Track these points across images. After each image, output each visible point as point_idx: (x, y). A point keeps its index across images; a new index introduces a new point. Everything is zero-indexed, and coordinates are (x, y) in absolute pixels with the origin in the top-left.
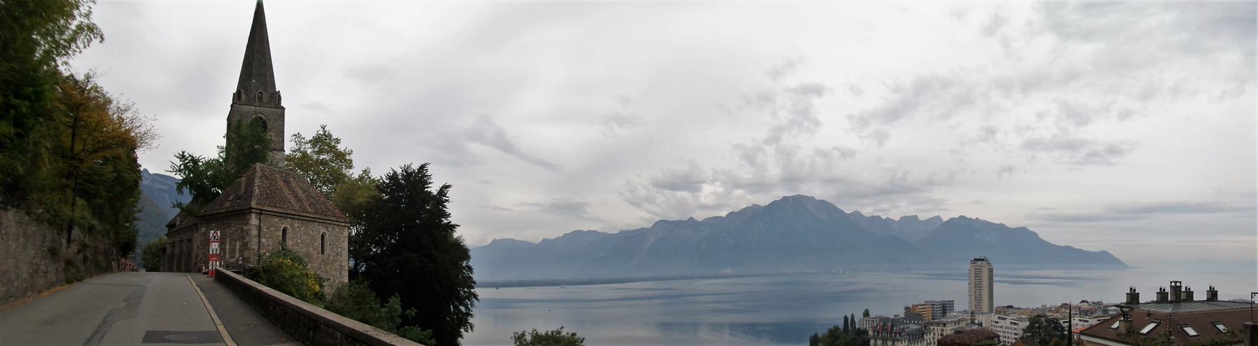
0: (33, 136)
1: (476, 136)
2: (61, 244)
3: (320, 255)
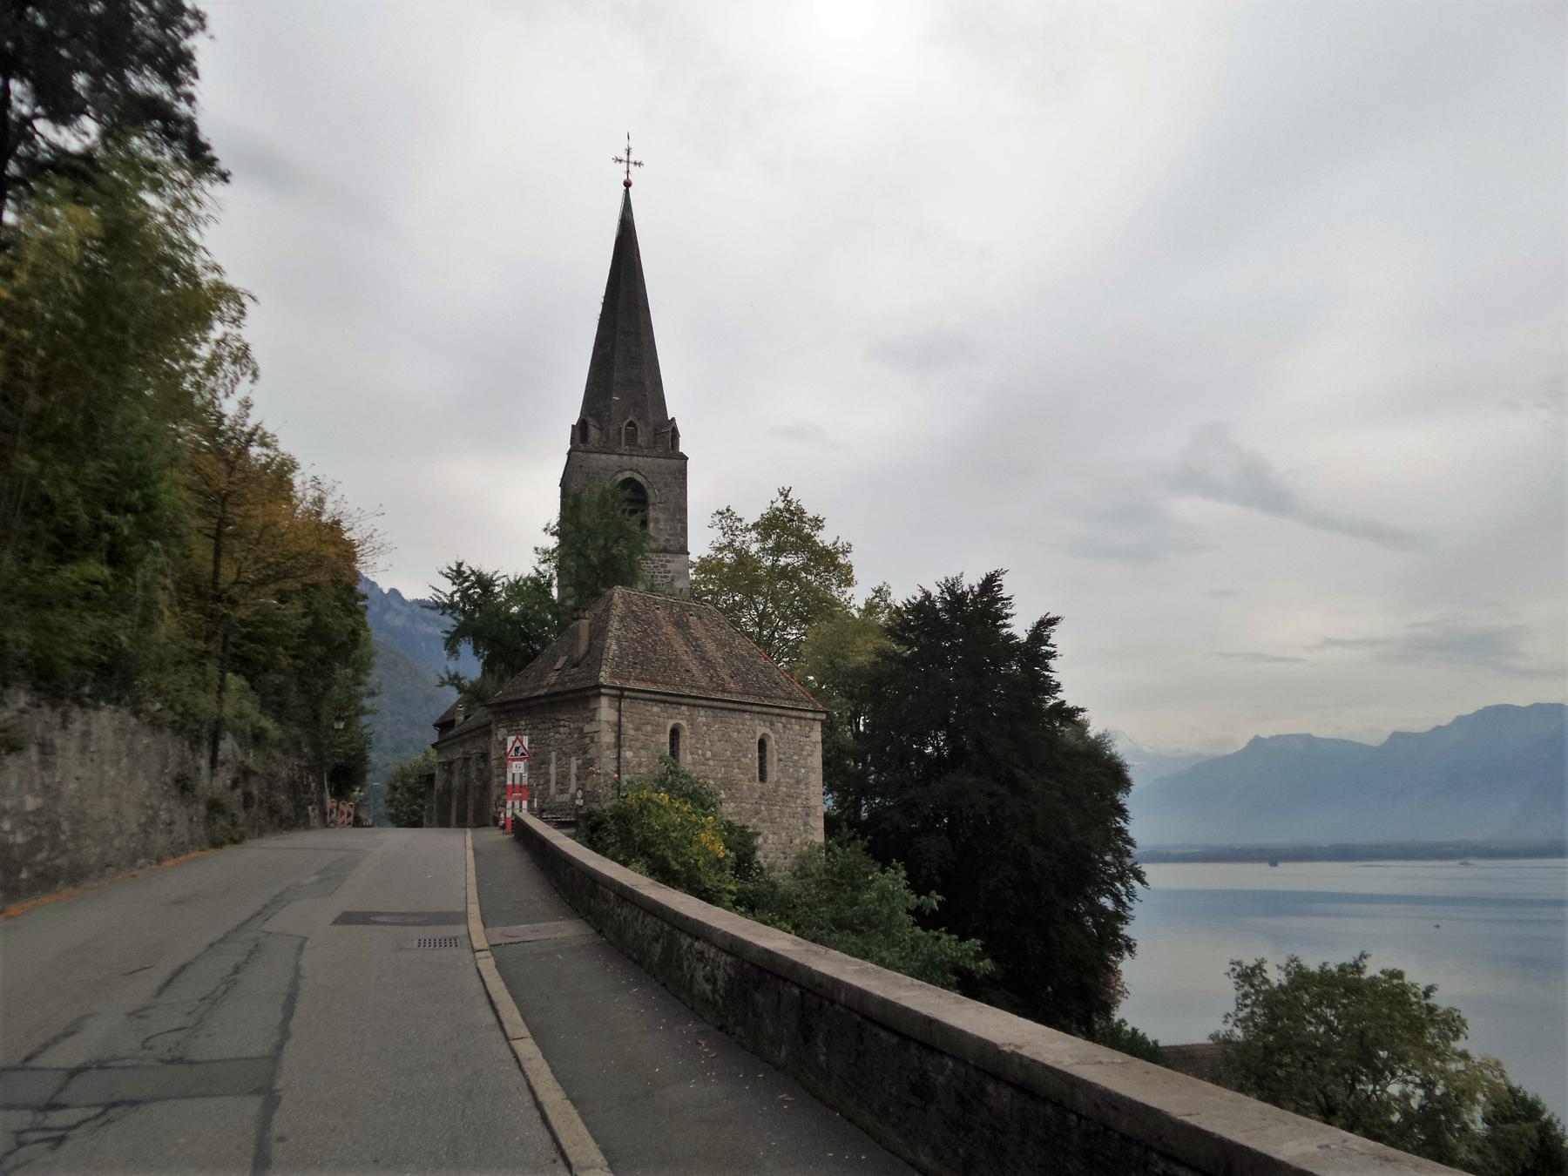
0: (142, 573)
1: (1191, 480)
2: (198, 769)
3: (757, 784)
